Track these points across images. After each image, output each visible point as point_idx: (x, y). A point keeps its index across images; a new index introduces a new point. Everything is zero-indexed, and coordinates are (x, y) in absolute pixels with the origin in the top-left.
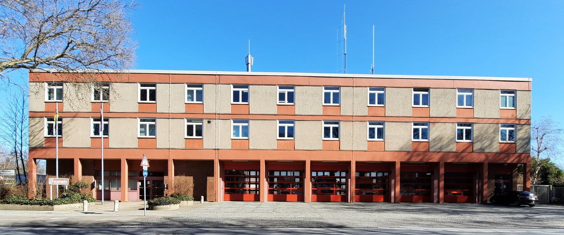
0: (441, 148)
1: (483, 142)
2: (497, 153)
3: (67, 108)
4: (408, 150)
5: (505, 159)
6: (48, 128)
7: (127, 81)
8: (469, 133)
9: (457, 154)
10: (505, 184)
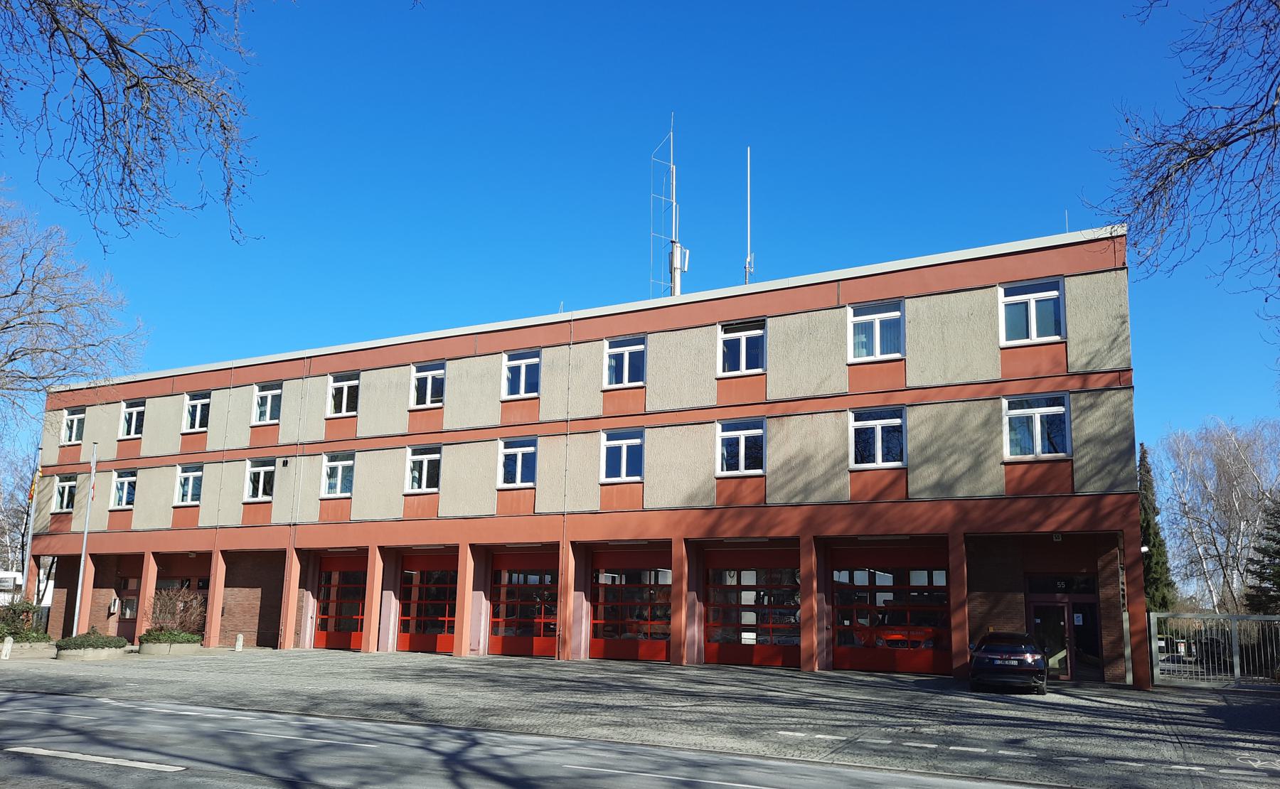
0: (807, 489)
1: (949, 462)
2: (995, 500)
3: (451, 420)
4: (705, 504)
5: (1035, 517)
6: (505, 465)
7: (835, 304)
8: (894, 437)
9: (857, 507)
10: (1076, 608)
